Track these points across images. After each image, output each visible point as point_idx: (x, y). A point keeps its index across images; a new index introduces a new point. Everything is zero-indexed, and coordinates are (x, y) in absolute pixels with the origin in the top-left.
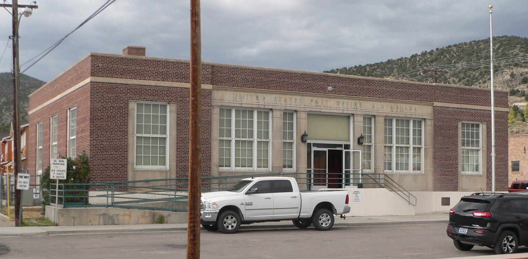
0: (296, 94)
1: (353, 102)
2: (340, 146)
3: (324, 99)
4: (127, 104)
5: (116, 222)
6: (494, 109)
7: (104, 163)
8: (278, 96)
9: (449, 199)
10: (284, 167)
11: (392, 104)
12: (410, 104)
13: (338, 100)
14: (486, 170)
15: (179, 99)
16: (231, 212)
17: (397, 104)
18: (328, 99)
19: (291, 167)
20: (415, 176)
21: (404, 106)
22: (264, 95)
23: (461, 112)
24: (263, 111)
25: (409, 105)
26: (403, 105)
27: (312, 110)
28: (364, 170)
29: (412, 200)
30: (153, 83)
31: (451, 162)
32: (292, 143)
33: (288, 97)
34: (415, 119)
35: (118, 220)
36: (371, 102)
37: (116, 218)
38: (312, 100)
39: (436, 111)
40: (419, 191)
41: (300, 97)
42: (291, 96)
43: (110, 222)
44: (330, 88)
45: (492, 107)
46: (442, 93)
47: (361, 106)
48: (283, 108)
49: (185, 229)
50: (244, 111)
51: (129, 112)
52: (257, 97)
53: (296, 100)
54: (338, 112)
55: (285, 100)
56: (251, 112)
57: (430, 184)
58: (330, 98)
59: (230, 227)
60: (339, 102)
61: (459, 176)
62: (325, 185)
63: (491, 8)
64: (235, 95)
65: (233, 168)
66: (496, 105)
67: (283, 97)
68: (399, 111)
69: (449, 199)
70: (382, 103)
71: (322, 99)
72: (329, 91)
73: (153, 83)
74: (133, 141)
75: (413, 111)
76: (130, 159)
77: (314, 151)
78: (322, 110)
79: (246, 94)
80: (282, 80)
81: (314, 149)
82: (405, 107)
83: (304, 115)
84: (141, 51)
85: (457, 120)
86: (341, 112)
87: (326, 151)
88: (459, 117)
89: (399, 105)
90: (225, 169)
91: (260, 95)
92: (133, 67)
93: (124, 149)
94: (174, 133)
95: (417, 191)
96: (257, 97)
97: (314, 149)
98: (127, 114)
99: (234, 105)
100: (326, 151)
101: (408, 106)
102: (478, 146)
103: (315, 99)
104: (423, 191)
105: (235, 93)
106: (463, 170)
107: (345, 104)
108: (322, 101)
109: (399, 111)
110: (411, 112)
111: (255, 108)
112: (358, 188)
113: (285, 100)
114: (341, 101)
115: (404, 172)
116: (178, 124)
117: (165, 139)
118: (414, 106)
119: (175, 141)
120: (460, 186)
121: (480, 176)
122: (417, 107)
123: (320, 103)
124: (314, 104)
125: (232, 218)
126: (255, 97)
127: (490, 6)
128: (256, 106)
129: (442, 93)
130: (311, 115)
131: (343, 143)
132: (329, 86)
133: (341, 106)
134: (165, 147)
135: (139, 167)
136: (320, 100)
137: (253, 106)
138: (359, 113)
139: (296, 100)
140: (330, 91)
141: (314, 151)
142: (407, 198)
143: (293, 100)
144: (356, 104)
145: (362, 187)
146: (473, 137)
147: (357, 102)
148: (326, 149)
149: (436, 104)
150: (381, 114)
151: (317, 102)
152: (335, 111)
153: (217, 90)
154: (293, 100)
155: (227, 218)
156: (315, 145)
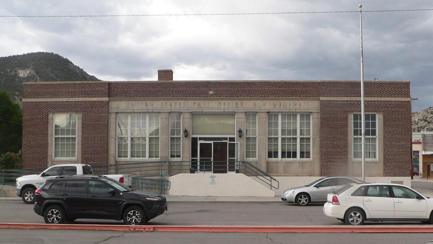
0: (180, 99)
1: (234, 102)
2: (226, 139)
3: (206, 102)
4: (48, 116)
5: (8, 195)
6: (364, 99)
7: (31, 156)
8: (164, 102)
10: (172, 156)
11: (275, 102)
12: (254, 100)
13: (220, 101)
14: (382, 157)
15: (83, 109)
16: (29, 189)
17: (280, 101)
18: (210, 101)
19: (179, 156)
20: (302, 164)
21: (288, 102)
22: (152, 102)
24: (305, 114)
25: (293, 101)
26: (286, 102)
27: (195, 111)
28: (366, 159)
29: (274, 184)
30: (65, 100)
31: (339, 150)
32: (74, 139)
33: (173, 102)
35: (9, 193)
36: (253, 101)
37: (8, 192)
38: (195, 103)
39: (324, 106)
40: (307, 176)
41: (184, 101)
42: (176, 101)
43: (4, 195)
44: (211, 92)
45: (362, 98)
46: (328, 89)
47: (242, 105)
51: (49, 121)
52: (146, 104)
53: (180, 104)
54: (219, 111)
55: (171, 104)
56: (295, 115)
57: (381, 171)
58: (212, 100)
59: (29, 199)
60: (220, 103)
62: (211, 171)
63: (361, 7)
64: (128, 104)
65: (129, 158)
66: (366, 95)
67: (169, 102)
70: (264, 102)
71: (204, 101)
72: (210, 95)
73: (65, 100)
74: (52, 140)
75: (298, 106)
76: (49, 153)
77: (200, 144)
78: (204, 111)
79: (137, 102)
80: (168, 89)
83: (187, 116)
85: (347, 112)
86: (222, 111)
87: (211, 144)
89: (282, 102)
90: (123, 159)
91: (148, 102)
92: (51, 90)
93: (45, 146)
94: (80, 134)
95: (305, 176)
96: (146, 104)
97: (199, 142)
98: (47, 122)
99: (280, 111)
100: (211, 144)
101: (292, 102)
103: (197, 102)
104: (311, 176)
105: (128, 102)
107: (227, 105)
108: (204, 103)
110: (296, 107)
111: (279, 112)
112: (236, 173)
113: (171, 104)
114: (222, 102)
115: (291, 159)
116: (83, 128)
117: (309, 138)
118: (298, 102)
119: (81, 139)
121: (376, 162)
122: (302, 102)
123: (202, 105)
124: (196, 106)
125: (31, 193)
126: (144, 104)
127: (359, 5)
128: (299, 111)
129: (328, 89)
130: (193, 115)
131: (228, 136)
132: (210, 90)
133: (222, 106)
134: (375, 145)
135: (57, 158)
136: (202, 103)
137: (297, 111)
138: (240, 111)
139: (180, 104)
140: (212, 95)
141: (200, 144)
142: (269, 183)
143: (178, 104)
144: (237, 104)
145: (238, 173)
147: (238, 102)
148: (212, 142)
149: (322, 98)
150: (263, 111)
151: (199, 104)
153: (114, 101)
154: (178, 104)
155: (31, 193)
156: (201, 139)
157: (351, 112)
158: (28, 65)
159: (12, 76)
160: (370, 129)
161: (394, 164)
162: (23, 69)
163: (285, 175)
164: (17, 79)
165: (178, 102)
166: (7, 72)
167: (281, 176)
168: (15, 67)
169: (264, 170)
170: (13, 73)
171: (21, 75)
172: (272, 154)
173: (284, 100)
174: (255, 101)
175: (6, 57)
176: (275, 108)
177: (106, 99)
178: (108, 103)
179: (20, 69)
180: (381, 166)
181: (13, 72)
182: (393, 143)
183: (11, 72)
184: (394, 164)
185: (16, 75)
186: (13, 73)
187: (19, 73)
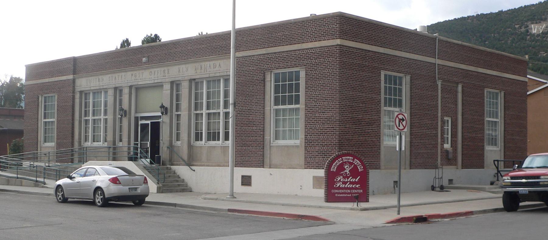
9: (250, 177)
18: (144, 71)
21: (208, 63)
23: (268, 58)
26: (207, 63)
31: (254, 128)
34: (95, 91)
46: (245, 39)
48: (114, 86)
49: (500, 198)
50: (214, 81)
60: (151, 72)
61: (267, 148)
68: (203, 71)
69: (250, 177)
72: (144, 63)
81: (140, 122)
82: (208, 65)
84: (156, 38)
86: (152, 82)
88: (266, 66)
97: (140, 122)
102: (297, 102)
106: (277, 138)
109: (203, 71)
118: (217, 63)
120: (267, 161)
129: (245, 39)
132: (144, 57)
144: (164, 71)
146: (395, 84)
148: (149, 122)
152: (148, 82)
157: (270, 70)
158: (543, 17)
159: (522, 33)
160: (280, 95)
161: (317, 148)
162: (536, 23)
163: (208, 164)
164: (528, 37)
165: (120, 74)
166: (515, 28)
167: (204, 166)
168: (526, 22)
169: (185, 157)
170: (523, 30)
171: (534, 31)
172: (198, 137)
173: (204, 61)
174: (180, 66)
175: (515, 9)
176: (196, 73)
177: (71, 77)
178: (74, 81)
179: (532, 23)
180: (302, 152)
181: (523, 27)
182: (317, 115)
183: (520, 27)
184: (317, 148)
185: (527, 31)
186: (523, 30)
187: (531, 29)
